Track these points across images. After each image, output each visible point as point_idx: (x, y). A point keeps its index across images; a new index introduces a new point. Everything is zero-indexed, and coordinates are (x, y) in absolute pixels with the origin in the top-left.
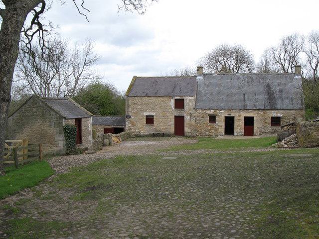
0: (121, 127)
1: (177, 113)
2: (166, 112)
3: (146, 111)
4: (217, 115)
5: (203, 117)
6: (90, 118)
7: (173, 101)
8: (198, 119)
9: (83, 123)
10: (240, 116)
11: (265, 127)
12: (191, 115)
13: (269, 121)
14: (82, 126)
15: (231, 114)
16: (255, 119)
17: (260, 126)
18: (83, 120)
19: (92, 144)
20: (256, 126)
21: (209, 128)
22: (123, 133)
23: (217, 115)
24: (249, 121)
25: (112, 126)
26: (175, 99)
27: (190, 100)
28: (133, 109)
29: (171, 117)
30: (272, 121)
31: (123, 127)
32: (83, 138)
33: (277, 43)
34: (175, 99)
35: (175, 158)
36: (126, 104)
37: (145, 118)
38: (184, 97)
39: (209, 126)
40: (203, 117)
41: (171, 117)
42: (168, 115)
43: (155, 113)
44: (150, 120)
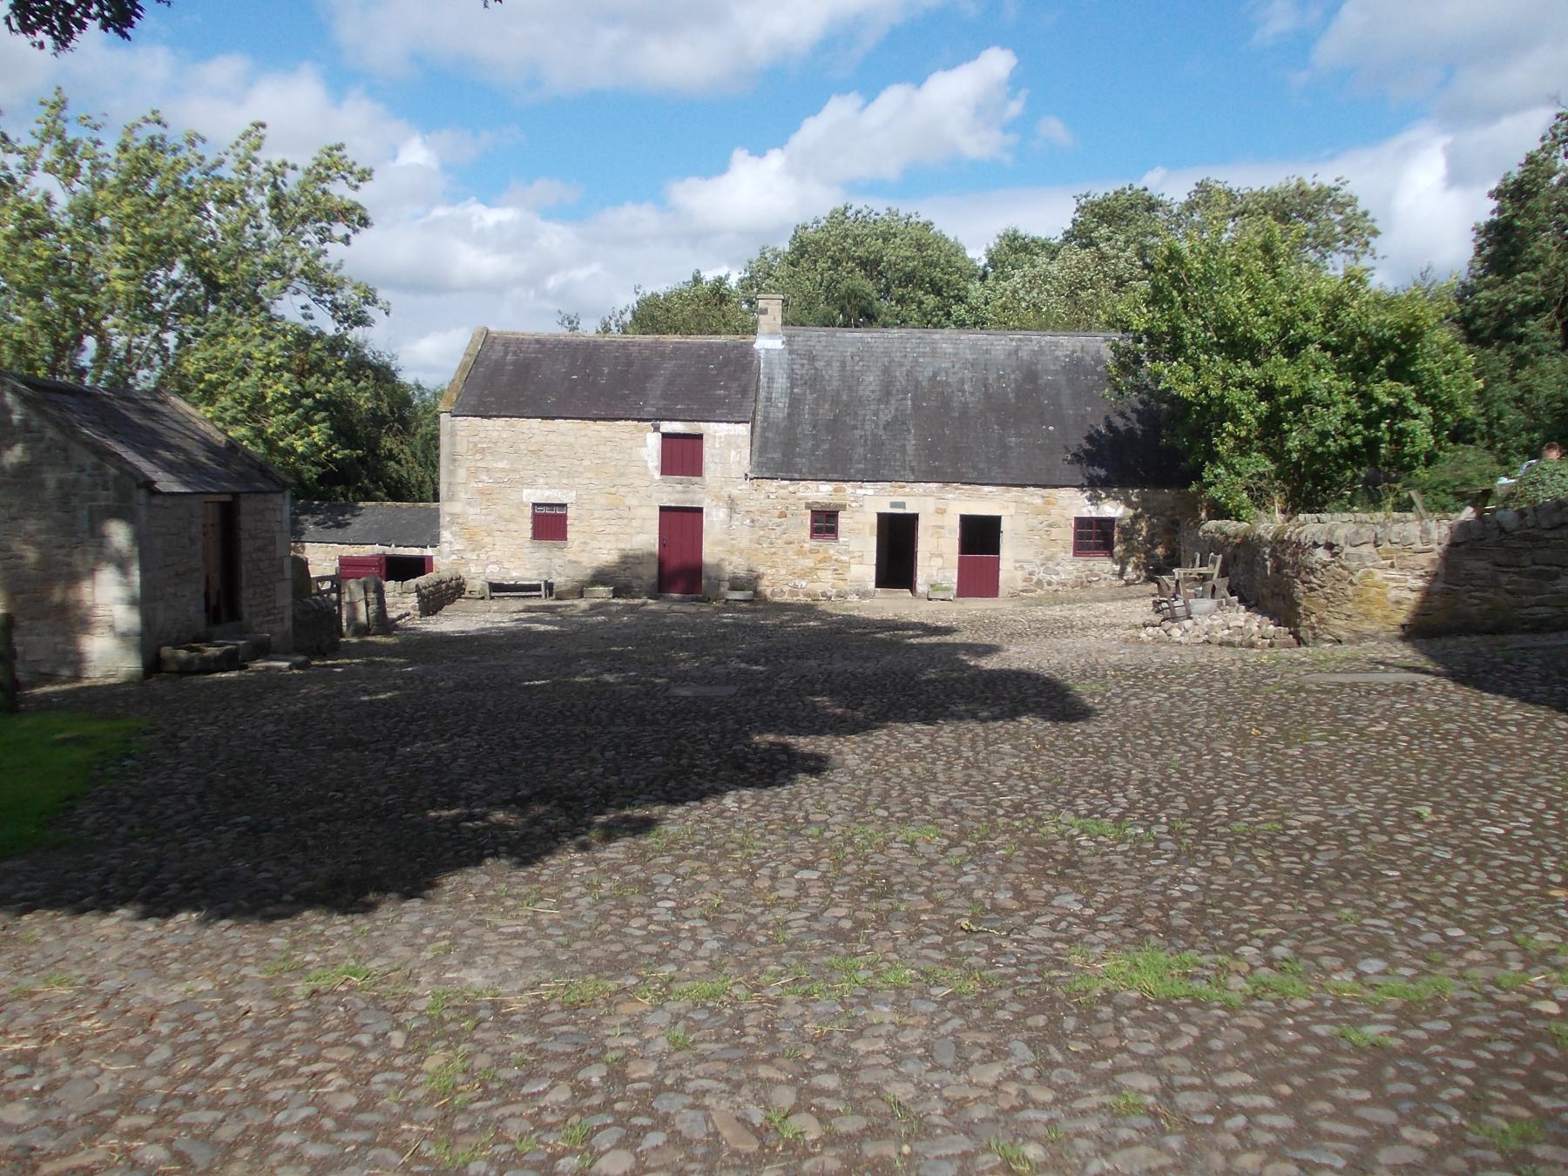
0: (416, 552)
1: (675, 493)
2: (622, 490)
3: (531, 485)
4: (843, 507)
5: (783, 515)
6: (278, 499)
7: (653, 441)
8: (764, 519)
9: (246, 522)
10: (941, 512)
11: (1048, 559)
12: (732, 505)
13: (1067, 535)
14: (243, 535)
15: (903, 505)
16: (1004, 526)
17: (1028, 554)
18: (245, 505)
19: (288, 624)
20: (1012, 559)
21: (809, 562)
22: (421, 580)
23: (843, 507)
24: (980, 537)
25: (377, 549)
26: (665, 436)
27: (730, 442)
28: (473, 474)
29: (644, 511)
30: (1079, 536)
31: (428, 552)
32: (246, 595)
33: (1473, 235)
34: (665, 436)
35: (732, 690)
36: (762, 394)
37: (529, 512)
38: (702, 427)
39: (811, 551)
40: (783, 515)
41: (644, 511)
42: (631, 501)
43: (573, 494)
44: (549, 524)
